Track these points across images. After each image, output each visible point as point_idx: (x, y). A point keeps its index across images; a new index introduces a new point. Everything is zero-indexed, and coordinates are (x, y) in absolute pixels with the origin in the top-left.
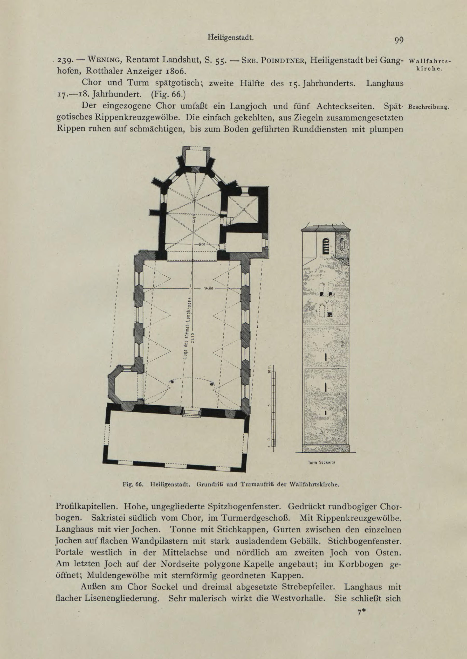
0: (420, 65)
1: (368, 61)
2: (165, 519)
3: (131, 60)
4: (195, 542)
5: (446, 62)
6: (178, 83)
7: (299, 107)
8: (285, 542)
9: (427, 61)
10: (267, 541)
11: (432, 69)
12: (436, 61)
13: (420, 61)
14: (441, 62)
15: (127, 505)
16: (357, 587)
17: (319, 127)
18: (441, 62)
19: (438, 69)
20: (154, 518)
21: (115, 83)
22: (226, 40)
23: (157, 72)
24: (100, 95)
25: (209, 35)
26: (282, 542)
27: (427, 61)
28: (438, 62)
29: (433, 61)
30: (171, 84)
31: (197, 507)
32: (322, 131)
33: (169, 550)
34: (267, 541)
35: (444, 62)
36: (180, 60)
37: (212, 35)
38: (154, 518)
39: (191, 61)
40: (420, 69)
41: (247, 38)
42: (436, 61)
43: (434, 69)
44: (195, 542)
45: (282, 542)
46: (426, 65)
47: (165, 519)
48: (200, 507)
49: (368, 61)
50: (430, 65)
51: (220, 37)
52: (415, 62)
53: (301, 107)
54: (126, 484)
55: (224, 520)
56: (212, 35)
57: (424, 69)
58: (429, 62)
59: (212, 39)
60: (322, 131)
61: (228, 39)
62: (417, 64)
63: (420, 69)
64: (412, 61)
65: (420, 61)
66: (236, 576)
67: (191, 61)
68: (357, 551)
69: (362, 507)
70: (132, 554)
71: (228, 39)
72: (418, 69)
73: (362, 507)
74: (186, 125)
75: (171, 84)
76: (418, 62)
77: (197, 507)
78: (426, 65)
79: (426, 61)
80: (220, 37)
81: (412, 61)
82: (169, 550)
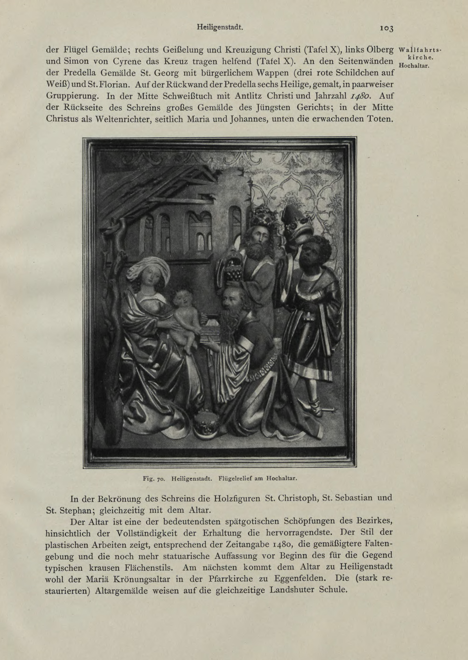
0: (411, 54)
4: (186, 73)
5: (438, 50)
6: (249, 522)
7: (262, 109)
8: (182, 511)
11: (423, 57)
12: (426, 50)
13: (410, 50)
14: (432, 51)
16: (248, 545)
17: (302, 117)
18: (432, 51)
19: (430, 57)
20: (181, 120)
21: (79, 84)
23: (366, 568)
25: (198, 25)
26: (179, 511)
28: (429, 51)
29: (424, 50)
30: (241, 522)
31: (74, 592)
32: (305, 120)
35: (435, 50)
36: (202, 522)
37: (202, 25)
38: (181, 120)
40: (412, 58)
42: (426, 50)
43: (425, 58)
44: (186, 73)
45: (179, 511)
48: (77, 591)
50: (422, 54)
52: (405, 50)
53: (265, 109)
56: (202, 25)
57: (415, 58)
58: (419, 50)
59: (202, 29)
60: (305, 120)
62: (408, 53)
63: (412, 58)
64: (402, 50)
65: (410, 50)
68: (264, 554)
72: (409, 58)
73: (295, 556)
74: (362, 539)
75: (241, 522)
76: (408, 51)
77: (74, 592)
79: (416, 50)
81: (402, 50)
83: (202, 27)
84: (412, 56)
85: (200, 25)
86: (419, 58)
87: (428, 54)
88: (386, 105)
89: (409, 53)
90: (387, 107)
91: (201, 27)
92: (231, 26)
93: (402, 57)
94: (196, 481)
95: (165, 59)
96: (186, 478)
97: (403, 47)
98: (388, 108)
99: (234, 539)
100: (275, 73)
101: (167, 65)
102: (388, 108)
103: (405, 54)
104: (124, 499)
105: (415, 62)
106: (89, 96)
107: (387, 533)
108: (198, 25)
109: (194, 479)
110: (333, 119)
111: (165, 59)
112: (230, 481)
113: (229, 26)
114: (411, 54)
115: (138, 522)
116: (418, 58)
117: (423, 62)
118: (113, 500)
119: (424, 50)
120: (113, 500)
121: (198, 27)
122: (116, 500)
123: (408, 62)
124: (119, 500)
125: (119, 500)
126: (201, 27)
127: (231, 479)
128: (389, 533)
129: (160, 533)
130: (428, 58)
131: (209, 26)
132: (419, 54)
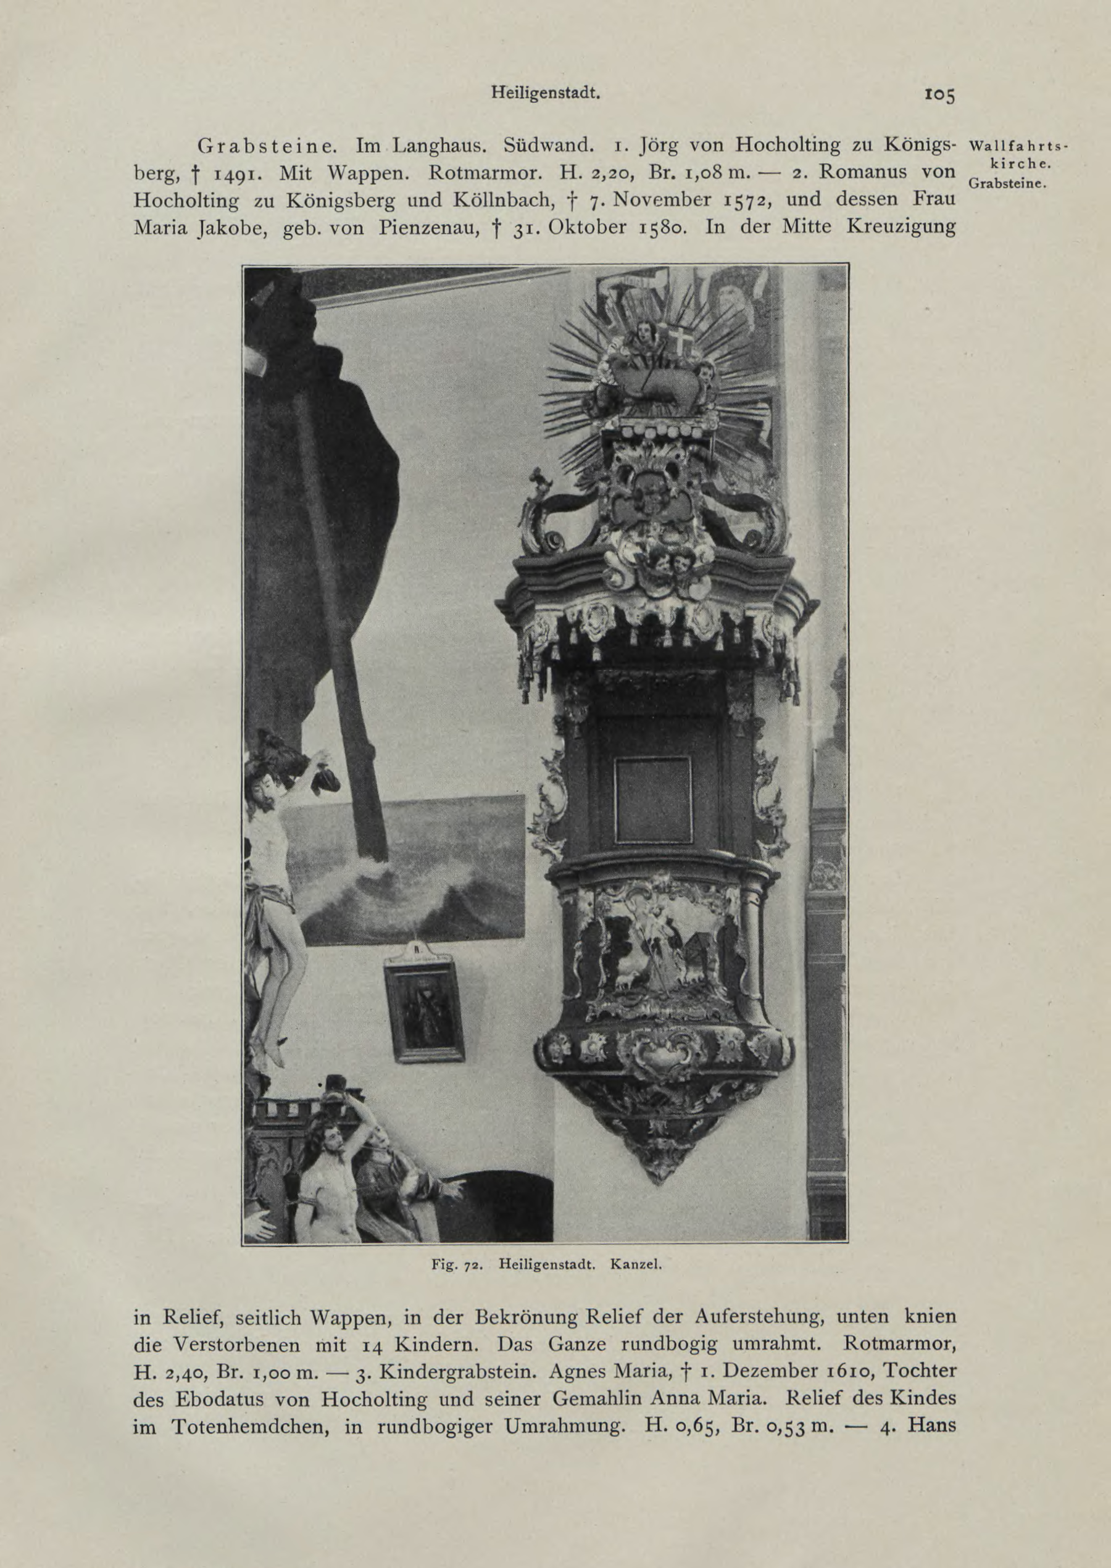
0: (998, 156)
1: (140, 174)
2: (699, 148)
3: (833, 172)
9: (1011, 145)
10: (272, 1346)
11: (1027, 164)
13: (993, 147)
15: (652, 1421)
22: (534, 100)
24: (607, 1400)
25: (494, 87)
27: (1011, 145)
28: (1037, 147)
29: (1026, 147)
32: (624, 1320)
33: (294, 167)
34: (272, 1346)
35: (1053, 147)
37: (502, 87)
39: (785, 1319)
40: (1000, 165)
41: (584, 94)
46: (1010, 156)
47: (699, 148)
49: (140, 174)
51: (522, 92)
54: (440, 1264)
55: (179, 1432)
56: (502, 87)
57: (1007, 165)
58: (1015, 147)
59: (502, 97)
60: (624, 1320)
61: (538, 97)
63: (1000, 165)
64: (975, 145)
66: (530, 173)
67: (785, 1319)
69: (457, 1427)
70: (410, 1321)
71: (538, 97)
72: (994, 165)
73: (457, 1427)
76: (988, 148)
78: (1010, 156)
79: (1007, 147)
80: (522, 92)
81: (975, 145)
82: (294, 167)
83: (502, 92)
84: (1000, 161)
85: (498, 89)
86: (1016, 165)
87: (1037, 156)
88: (814, 222)
89: (993, 153)
90: (817, 224)
91: (499, 91)
92: (571, 89)
93: (979, 165)
94: (559, 1271)
95: (457, 193)
96: (533, 1263)
97: (979, 140)
98: (820, 228)
99: (804, 1386)
100: (370, 174)
101: (462, 208)
102: (820, 228)
103: (984, 156)
104: (538, 1318)
105: (1004, 175)
106: (939, 227)
107: (944, 1373)
108: (494, 87)
109: (554, 1266)
110: (534, 201)
111: (457, 193)
112: (537, 1269)
113: (568, 90)
114: (998, 156)
115: (737, 1345)
116: (1015, 166)
117: (1032, 175)
118: (510, 1319)
119: (1026, 147)
120: (510, 1319)
121: (495, 92)
122: (518, 1319)
123: (989, 175)
124: (526, 1319)
125: (526, 1319)
126: (499, 91)
127: (541, 1266)
128: (949, 1372)
129: (454, 1425)
130: (1037, 165)
131: (519, 89)
132: (1016, 156)
